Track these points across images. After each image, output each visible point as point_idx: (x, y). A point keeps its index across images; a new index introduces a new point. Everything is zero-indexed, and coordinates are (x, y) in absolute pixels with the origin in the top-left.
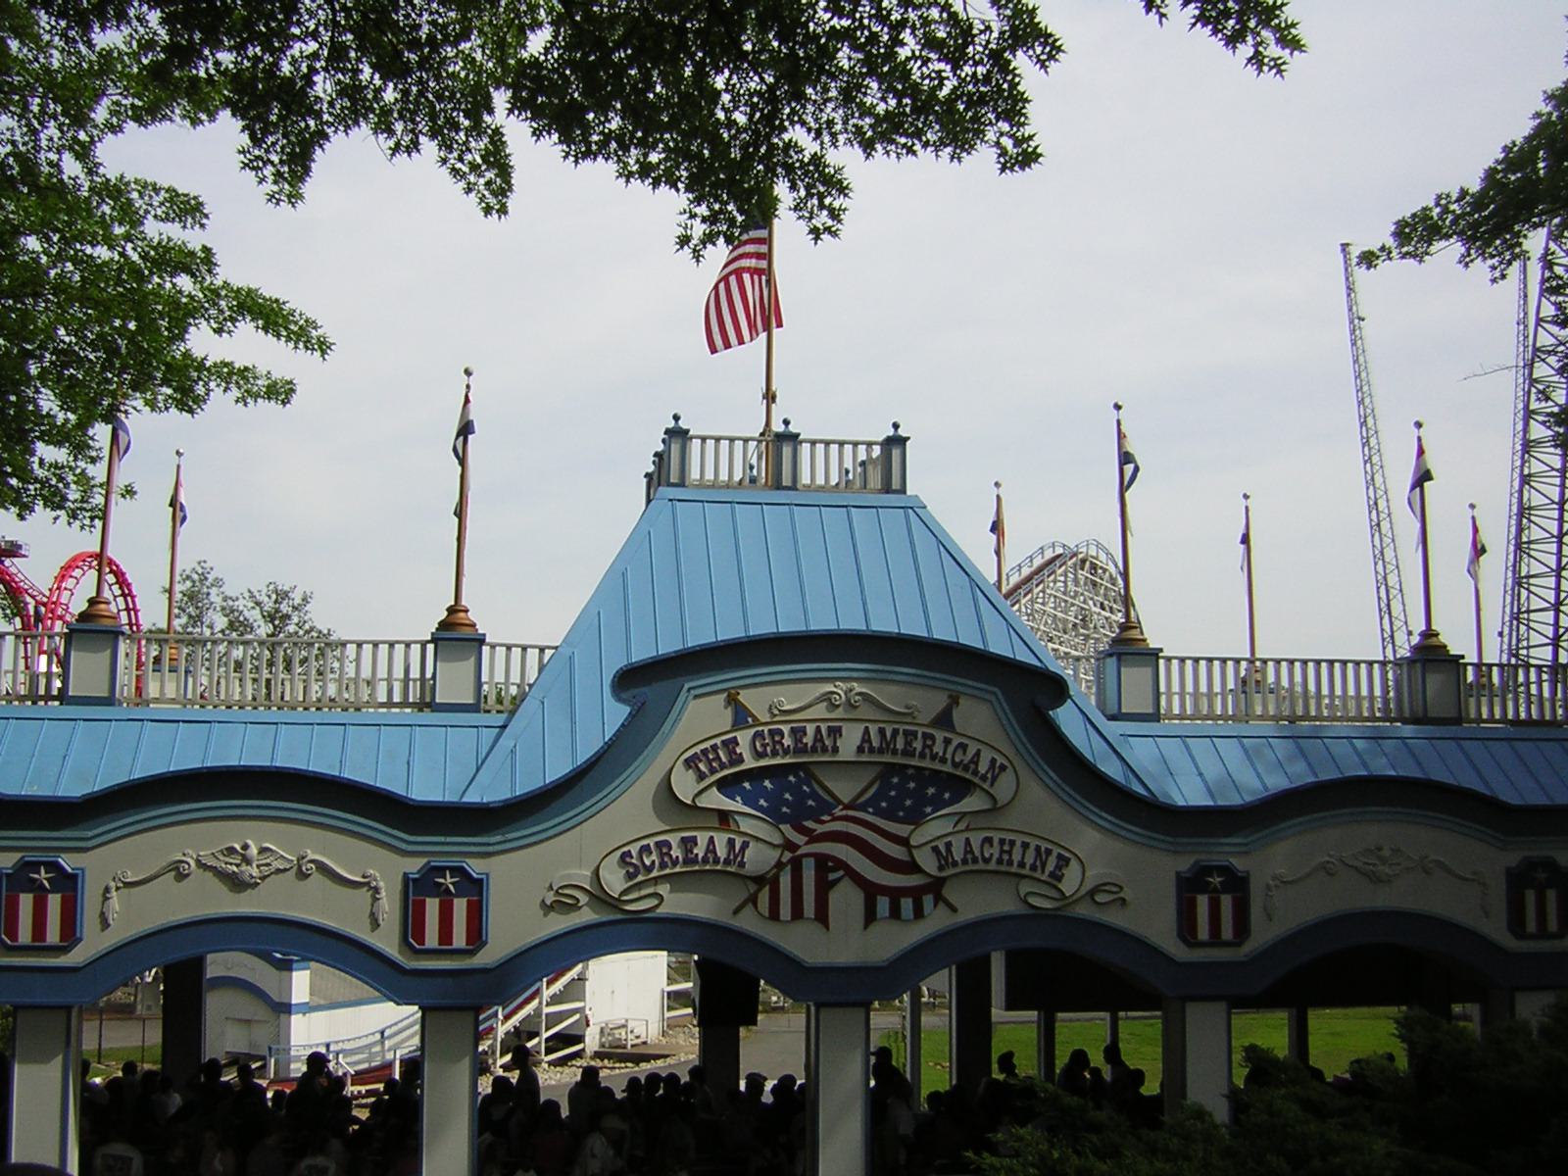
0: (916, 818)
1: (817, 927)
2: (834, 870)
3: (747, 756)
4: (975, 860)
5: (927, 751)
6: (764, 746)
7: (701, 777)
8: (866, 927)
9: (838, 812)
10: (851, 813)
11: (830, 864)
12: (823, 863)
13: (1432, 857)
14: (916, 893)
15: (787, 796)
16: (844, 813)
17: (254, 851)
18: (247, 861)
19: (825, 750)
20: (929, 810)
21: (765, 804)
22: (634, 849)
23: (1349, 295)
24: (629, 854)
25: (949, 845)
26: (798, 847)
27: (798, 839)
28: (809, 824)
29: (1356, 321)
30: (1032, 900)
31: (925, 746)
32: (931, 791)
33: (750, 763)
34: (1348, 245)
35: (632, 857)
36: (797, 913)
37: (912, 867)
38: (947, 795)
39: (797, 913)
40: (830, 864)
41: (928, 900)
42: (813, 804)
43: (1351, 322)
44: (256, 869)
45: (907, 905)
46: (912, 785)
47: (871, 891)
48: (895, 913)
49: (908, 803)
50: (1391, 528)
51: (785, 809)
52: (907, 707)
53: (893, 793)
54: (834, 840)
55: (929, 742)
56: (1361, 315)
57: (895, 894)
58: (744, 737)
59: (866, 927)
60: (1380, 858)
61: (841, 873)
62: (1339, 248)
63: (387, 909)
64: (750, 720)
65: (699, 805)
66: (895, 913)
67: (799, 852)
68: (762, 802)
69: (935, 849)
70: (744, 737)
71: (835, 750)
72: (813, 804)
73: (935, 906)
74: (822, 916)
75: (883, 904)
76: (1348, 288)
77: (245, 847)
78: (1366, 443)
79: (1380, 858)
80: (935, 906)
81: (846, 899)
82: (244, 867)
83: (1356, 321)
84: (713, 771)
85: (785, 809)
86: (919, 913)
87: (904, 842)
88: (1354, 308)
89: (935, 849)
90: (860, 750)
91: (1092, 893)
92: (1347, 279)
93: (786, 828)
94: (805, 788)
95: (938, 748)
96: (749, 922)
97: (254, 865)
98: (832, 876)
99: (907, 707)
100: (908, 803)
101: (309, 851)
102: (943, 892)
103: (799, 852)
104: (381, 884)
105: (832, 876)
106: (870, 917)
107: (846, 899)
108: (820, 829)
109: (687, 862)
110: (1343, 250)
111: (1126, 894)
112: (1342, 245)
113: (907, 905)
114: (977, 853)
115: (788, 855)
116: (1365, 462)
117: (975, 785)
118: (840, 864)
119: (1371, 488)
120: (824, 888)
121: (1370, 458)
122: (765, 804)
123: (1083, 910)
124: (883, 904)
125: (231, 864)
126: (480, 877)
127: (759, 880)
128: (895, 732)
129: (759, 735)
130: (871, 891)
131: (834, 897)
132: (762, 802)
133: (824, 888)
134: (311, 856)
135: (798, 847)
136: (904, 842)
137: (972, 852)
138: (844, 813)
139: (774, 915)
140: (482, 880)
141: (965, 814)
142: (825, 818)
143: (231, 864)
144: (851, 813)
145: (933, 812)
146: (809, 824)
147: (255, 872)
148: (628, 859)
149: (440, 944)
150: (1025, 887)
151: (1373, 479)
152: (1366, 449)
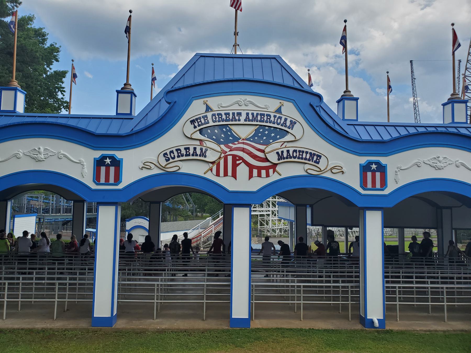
0: (267, 144)
1: (233, 179)
2: (238, 160)
3: (210, 121)
4: (291, 158)
5: (268, 120)
6: (216, 118)
7: (195, 127)
8: (249, 179)
9: (240, 141)
10: (244, 141)
11: (237, 158)
12: (235, 158)
13: (460, 161)
14: (267, 169)
15: (223, 135)
16: (242, 141)
17: (42, 150)
18: (40, 153)
19: (236, 120)
20: (271, 141)
21: (215, 138)
22: (168, 152)
23: (412, 73)
24: (166, 154)
25: (282, 152)
26: (227, 152)
27: (227, 150)
28: (230, 145)
29: (413, 79)
30: (309, 171)
31: (267, 118)
32: (273, 135)
33: (211, 124)
34: (412, 61)
35: (168, 155)
36: (226, 174)
37: (266, 160)
38: (278, 137)
39: (226, 174)
40: (237, 158)
41: (271, 171)
42: (232, 139)
43: (412, 80)
44: (43, 156)
45: (263, 172)
46: (267, 132)
47: (251, 167)
48: (259, 175)
49: (265, 138)
50: (418, 104)
51: (222, 140)
52: (265, 106)
53: (260, 135)
54: (236, 150)
55: (269, 117)
56: (415, 78)
57: (259, 169)
58: (209, 115)
59: (249, 179)
60: (439, 161)
61: (241, 161)
62: (410, 62)
63: (86, 172)
64: (210, 110)
65: (192, 137)
66: (259, 175)
67: (227, 154)
68: (214, 137)
69: (278, 153)
70: (209, 115)
71: (239, 120)
72: (232, 139)
73: (274, 173)
74: (234, 175)
75: (255, 172)
76: (412, 71)
77: (39, 149)
78: (413, 89)
79: (439, 161)
80: (274, 173)
81: (242, 170)
82: (39, 155)
83: (413, 79)
84: (199, 125)
85: (222, 140)
86: (268, 175)
87: (263, 151)
88: (413, 76)
89: (278, 153)
90: (245, 120)
91: (331, 169)
92: (411, 69)
93: (222, 146)
94: (229, 133)
95: (272, 119)
96: (211, 176)
97: (42, 154)
98: (238, 162)
99: (265, 106)
100: (265, 138)
101: (62, 151)
102: (276, 169)
103: (227, 154)
104: (85, 164)
105: (238, 162)
106: (251, 176)
107: (242, 170)
108: (234, 146)
109: (187, 155)
110: (411, 62)
111: (344, 169)
112: (410, 61)
113: (263, 172)
114: (291, 155)
115: (223, 155)
116: (415, 114)
117: (288, 132)
118: (241, 158)
119: (416, 120)
120: (235, 166)
121: (416, 112)
122: (215, 138)
123: (328, 175)
124: (255, 172)
125: (35, 154)
126: (119, 160)
127: (213, 163)
128: (257, 114)
129: (214, 115)
130: (251, 167)
131: (238, 168)
132: (214, 137)
133: (235, 166)
134: (62, 152)
135: (227, 152)
136: (263, 151)
137: (290, 155)
138: (242, 141)
139: (218, 174)
140: (120, 161)
141: (285, 142)
142: (236, 143)
143: (35, 154)
144: (244, 141)
145: (273, 142)
146: (230, 145)
147: (42, 156)
148: (166, 156)
149: (114, 183)
150: (307, 167)
151: (417, 117)
152: (415, 110)
